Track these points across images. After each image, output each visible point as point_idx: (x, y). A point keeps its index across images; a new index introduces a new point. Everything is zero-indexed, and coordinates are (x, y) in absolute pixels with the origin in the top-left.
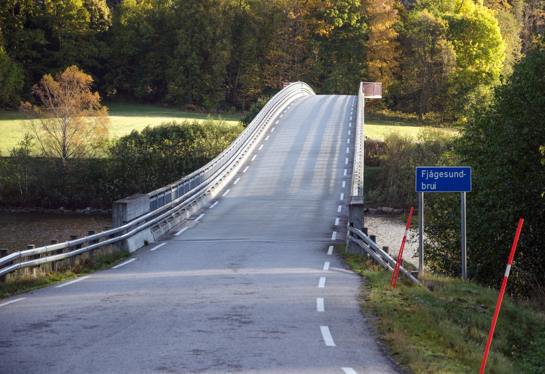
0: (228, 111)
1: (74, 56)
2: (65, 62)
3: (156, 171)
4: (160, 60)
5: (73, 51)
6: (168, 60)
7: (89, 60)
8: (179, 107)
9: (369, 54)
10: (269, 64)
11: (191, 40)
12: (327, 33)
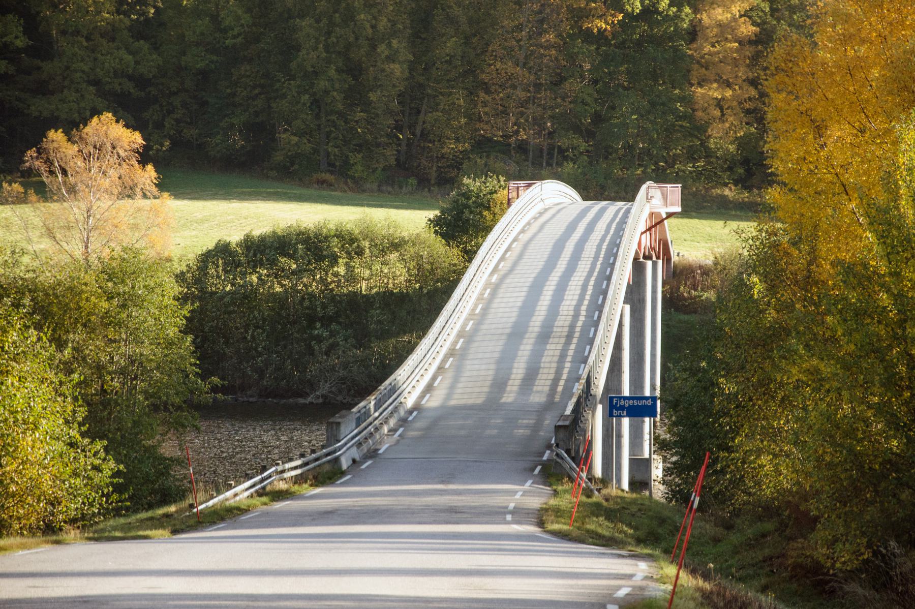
0: (401, 188)
1: (83, 72)
2: (66, 83)
3: (264, 320)
4: (262, 81)
5: (83, 60)
6: (279, 81)
7: (115, 80)
8: (300, 180)
9: (696, 73)
10: (488, 92)
11: (326, 40)
12: (608, 27)
